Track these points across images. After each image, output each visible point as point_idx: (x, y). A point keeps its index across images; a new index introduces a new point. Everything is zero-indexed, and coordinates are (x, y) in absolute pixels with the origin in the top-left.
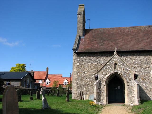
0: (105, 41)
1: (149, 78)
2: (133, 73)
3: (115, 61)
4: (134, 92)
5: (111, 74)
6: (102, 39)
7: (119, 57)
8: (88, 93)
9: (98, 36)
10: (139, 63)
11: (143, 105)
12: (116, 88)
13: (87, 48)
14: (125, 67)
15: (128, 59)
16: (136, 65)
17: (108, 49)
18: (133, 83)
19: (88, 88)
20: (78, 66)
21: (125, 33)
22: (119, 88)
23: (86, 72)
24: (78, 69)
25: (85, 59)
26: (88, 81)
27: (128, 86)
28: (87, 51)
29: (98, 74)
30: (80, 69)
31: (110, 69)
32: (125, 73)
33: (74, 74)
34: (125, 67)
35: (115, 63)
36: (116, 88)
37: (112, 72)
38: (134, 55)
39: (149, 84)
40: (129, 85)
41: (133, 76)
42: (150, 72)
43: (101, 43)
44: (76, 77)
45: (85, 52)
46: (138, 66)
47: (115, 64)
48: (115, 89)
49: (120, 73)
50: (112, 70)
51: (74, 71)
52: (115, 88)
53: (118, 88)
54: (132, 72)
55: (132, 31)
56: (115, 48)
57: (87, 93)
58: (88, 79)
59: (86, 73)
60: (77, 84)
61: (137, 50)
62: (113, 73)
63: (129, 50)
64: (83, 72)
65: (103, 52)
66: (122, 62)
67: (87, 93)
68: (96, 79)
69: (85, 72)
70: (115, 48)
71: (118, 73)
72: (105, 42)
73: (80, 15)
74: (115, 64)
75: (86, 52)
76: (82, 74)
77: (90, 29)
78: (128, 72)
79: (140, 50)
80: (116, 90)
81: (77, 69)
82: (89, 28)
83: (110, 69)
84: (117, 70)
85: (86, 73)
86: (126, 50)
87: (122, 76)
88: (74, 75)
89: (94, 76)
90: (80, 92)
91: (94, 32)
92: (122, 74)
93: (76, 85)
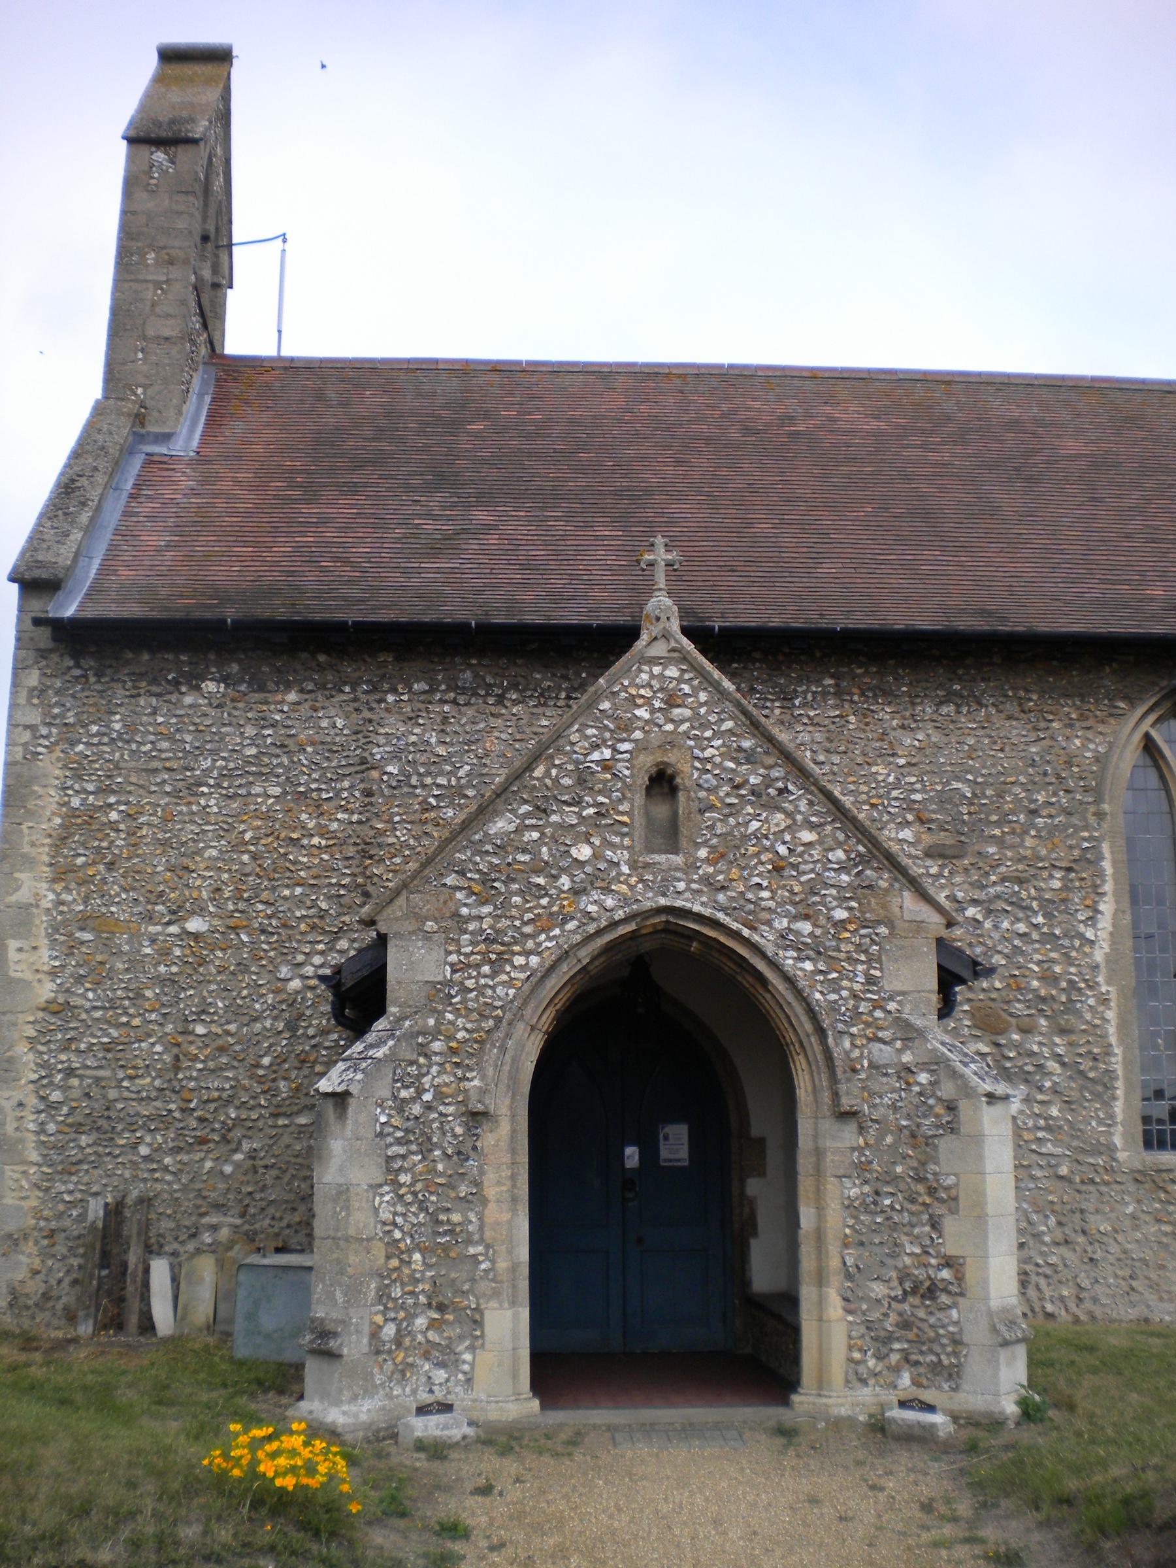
0: (484, 498)
1: (1078, 1014)
2: (918, 926)
3: (655, 737)
4: (949, 1224)
5: (590, 938)
6: (441, 480)
7: (716, 685)
8: (224, 1234)
9: (384, 445)
10: (945, 799)
11: (829, 1329)
12: (632, 1155)
13: (223, 574)
14: (807, 836)
15: (816, 724)
16: (906, 834)
17: (528, 596)
18: (923, 1078)
19: (224, 1148)
20: (79, 824)
21: (747, 430)
22: (675, 1144)
23: (201, 911)
24: (74, 869)
25: (207, 720)
26: (222, 1049)
27: (849, 1136)
28: (230, 614)
29: (382, 940)
30: (111, 866)
31: (583, 852)
32: (806, 927)
33: (13, 944)
34: (807, 836)
35: (647, 761)
36: (632, 1155)
37: (602, 905)
38: (885, 693)
39: (1072, 1088)
40: (846, 1103)
41: (918, 977)
42: (1090, 934)
43: (429, 526)
44: (46, 990)
45: (197, 615)
46: (928, 839)
47: (662, 782)
48: (663, 1159)
49: (721, 916)
50: (598, 878)
51: (23, 895)
52: (621, 1157)
53: (664, 1153)
54: (909, 904)
55: (834, 420)
56: (659, 540)
57: (207, 1238)
58: (235, 1012)
59: (196, 936)
60: (65, 1088)
61: (925, 621)
62: (614, 924)
63: (823, 624)
64: (150, 918)
65: (460, 629)
66: (750, 758)
67: (214, 1228)
68: (338, 1014)
69: (177, 914)
70: (659, 540)
71: (699, 918)
72: (480, 515)
73: (160, 156)
74: (662, 782)
75: (208, 615)
76: (135, 936)
77: (285, 353)
78: (840, 914)
79: (966, 623)
80: (629, 1181)
81: (61, 874)
82: (271, 352)
83: (583, 852)
84: (685, 888)
85: (195, 925)
86: (776, 622)
87: (761, 965)
88: (13, 955)
89: (320, 963)
90: (96, 1210)
91: (331, 394)
92: (766, 939)
93: (32, 1101)
